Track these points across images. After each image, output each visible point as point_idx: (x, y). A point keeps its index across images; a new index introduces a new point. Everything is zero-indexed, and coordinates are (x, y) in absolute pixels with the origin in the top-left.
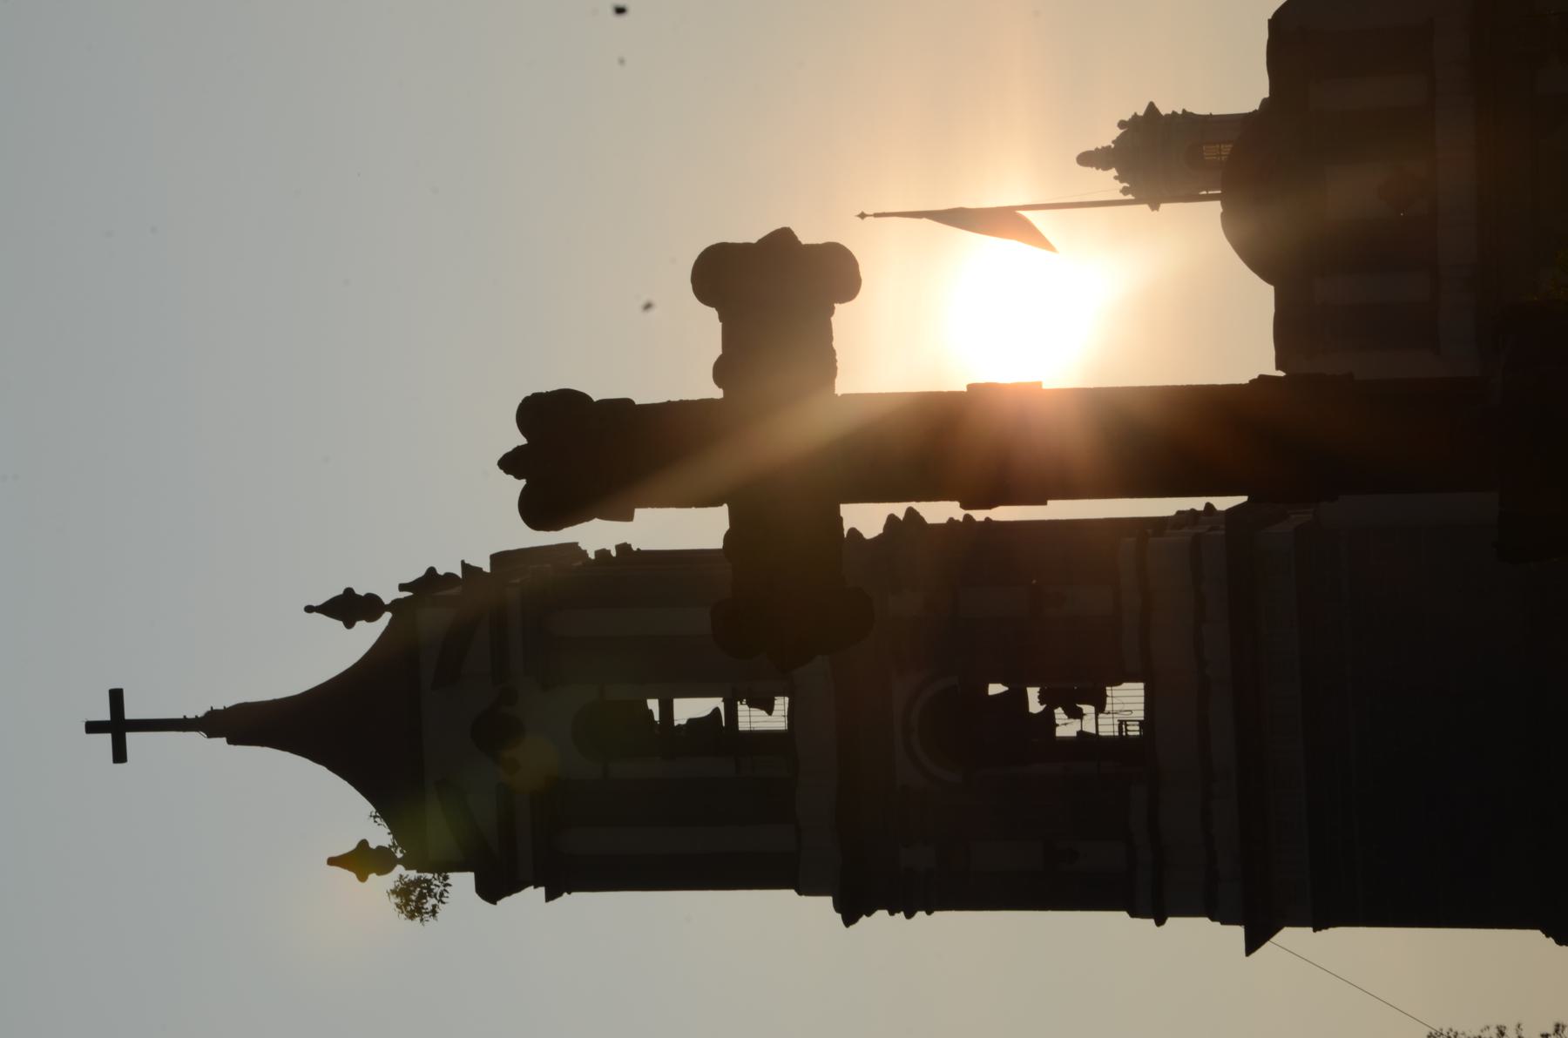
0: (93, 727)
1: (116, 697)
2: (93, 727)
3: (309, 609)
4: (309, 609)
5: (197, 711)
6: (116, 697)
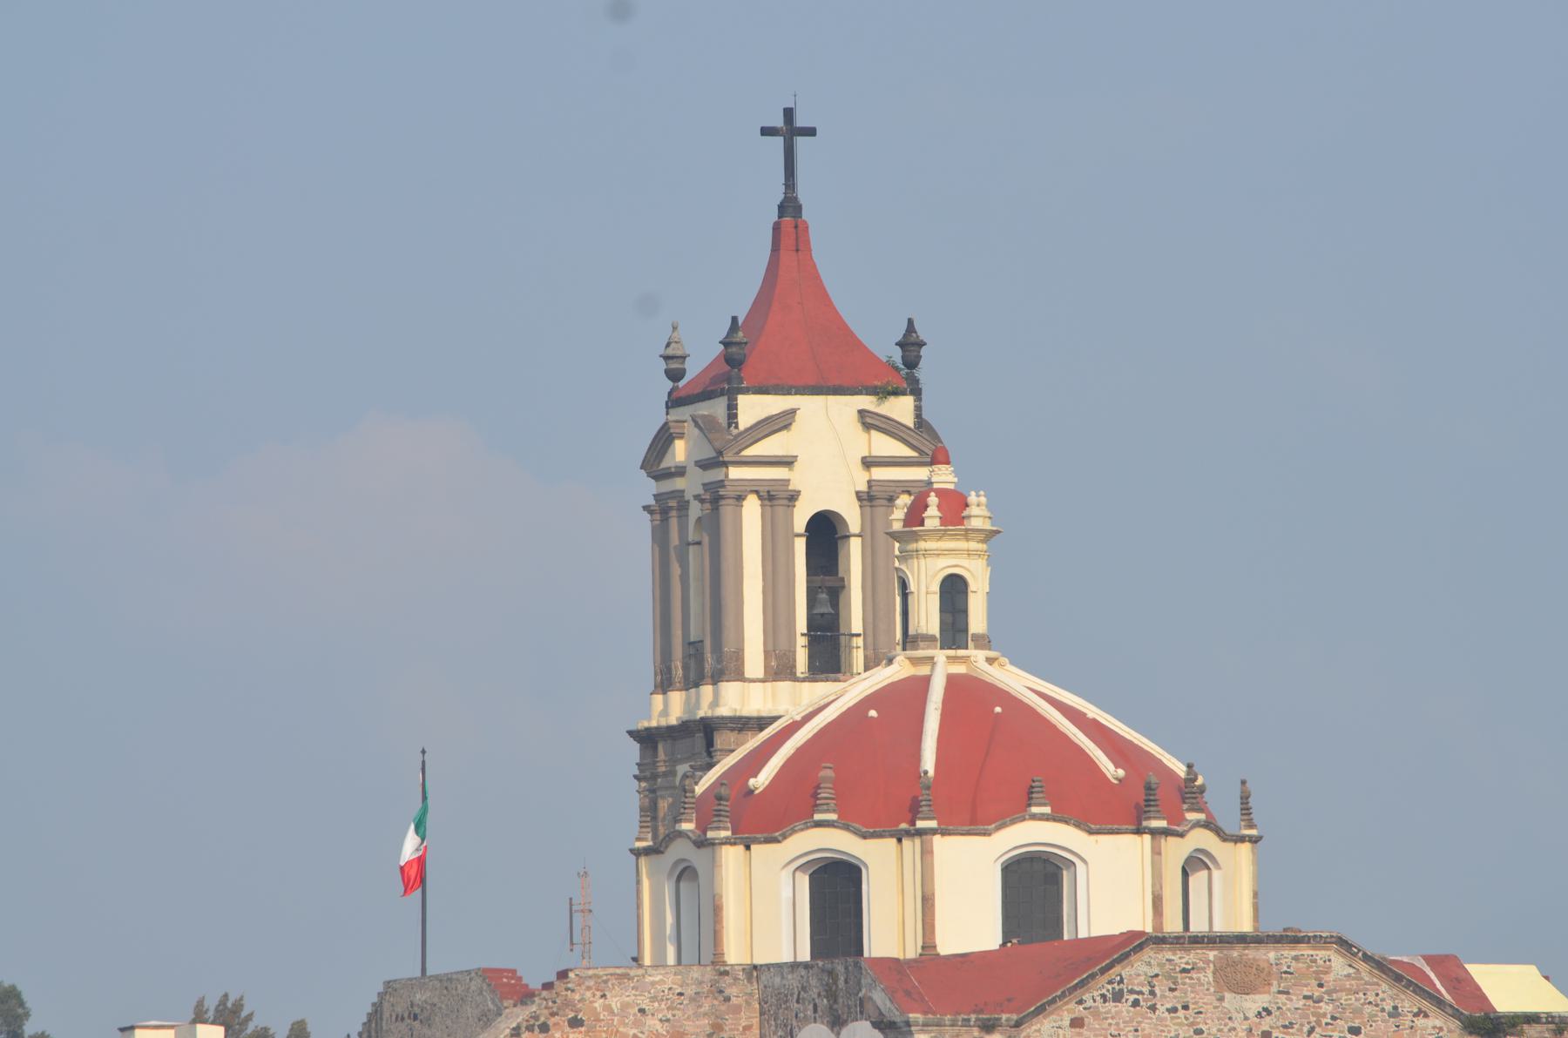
0: (789, 114)
1: (811, 132)
2: (789, 114)
3: (1243, 783)
4: (1243, 783)
5: (802, 194)
6: (811, 132)
